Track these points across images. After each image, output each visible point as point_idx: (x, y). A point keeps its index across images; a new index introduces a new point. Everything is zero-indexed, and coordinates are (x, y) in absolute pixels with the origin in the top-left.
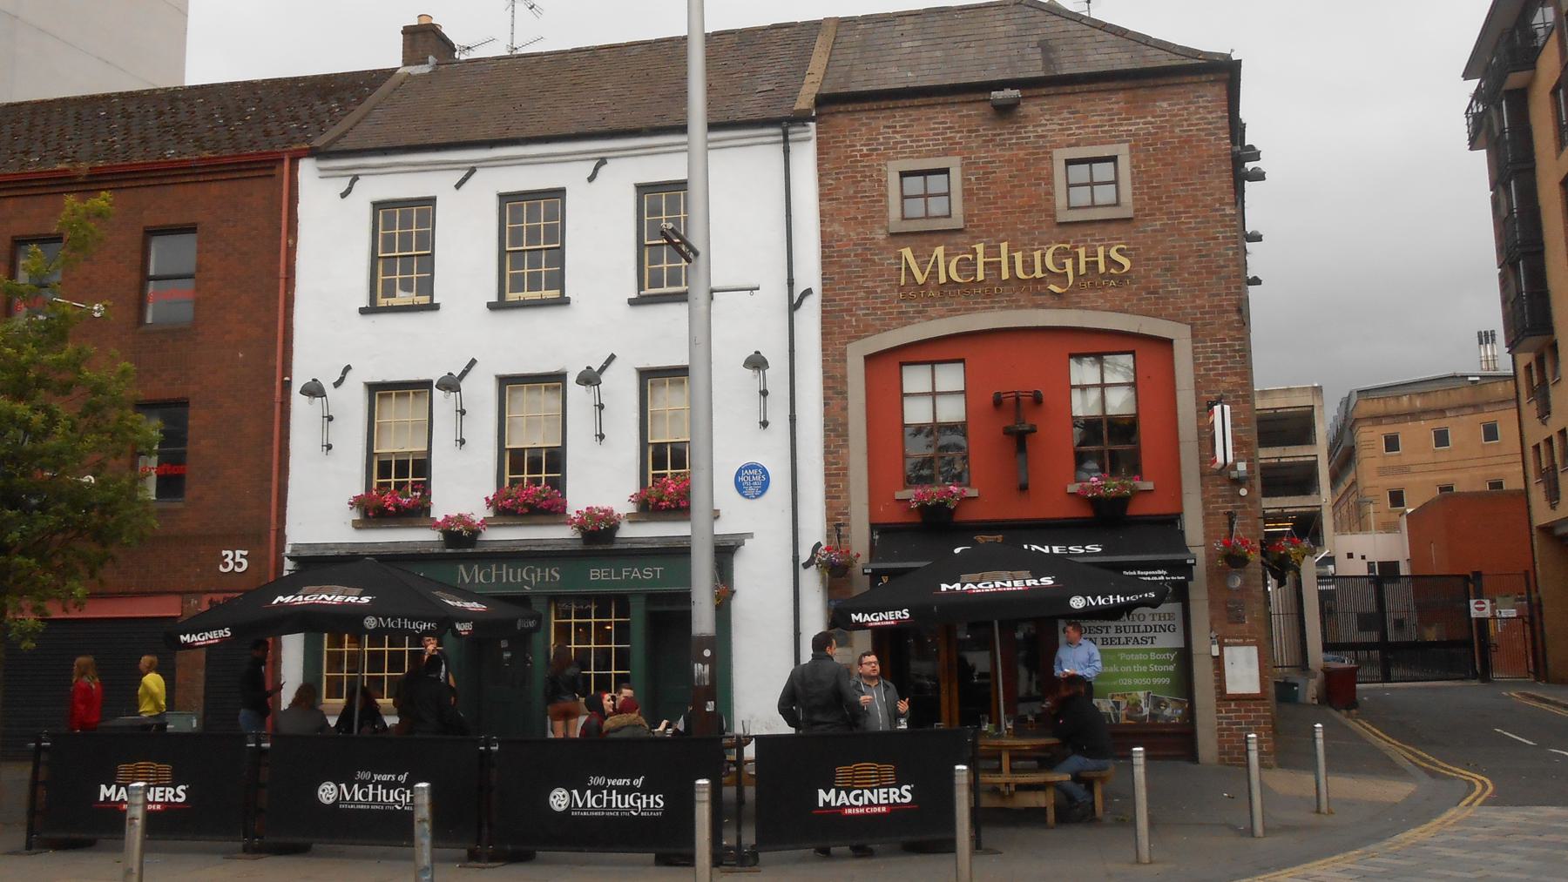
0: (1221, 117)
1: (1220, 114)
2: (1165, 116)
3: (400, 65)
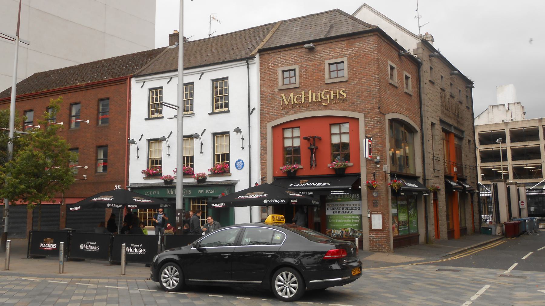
0: (375, 46)
1: (375, 45)
2: (358, 47)
3: (169, 46)
